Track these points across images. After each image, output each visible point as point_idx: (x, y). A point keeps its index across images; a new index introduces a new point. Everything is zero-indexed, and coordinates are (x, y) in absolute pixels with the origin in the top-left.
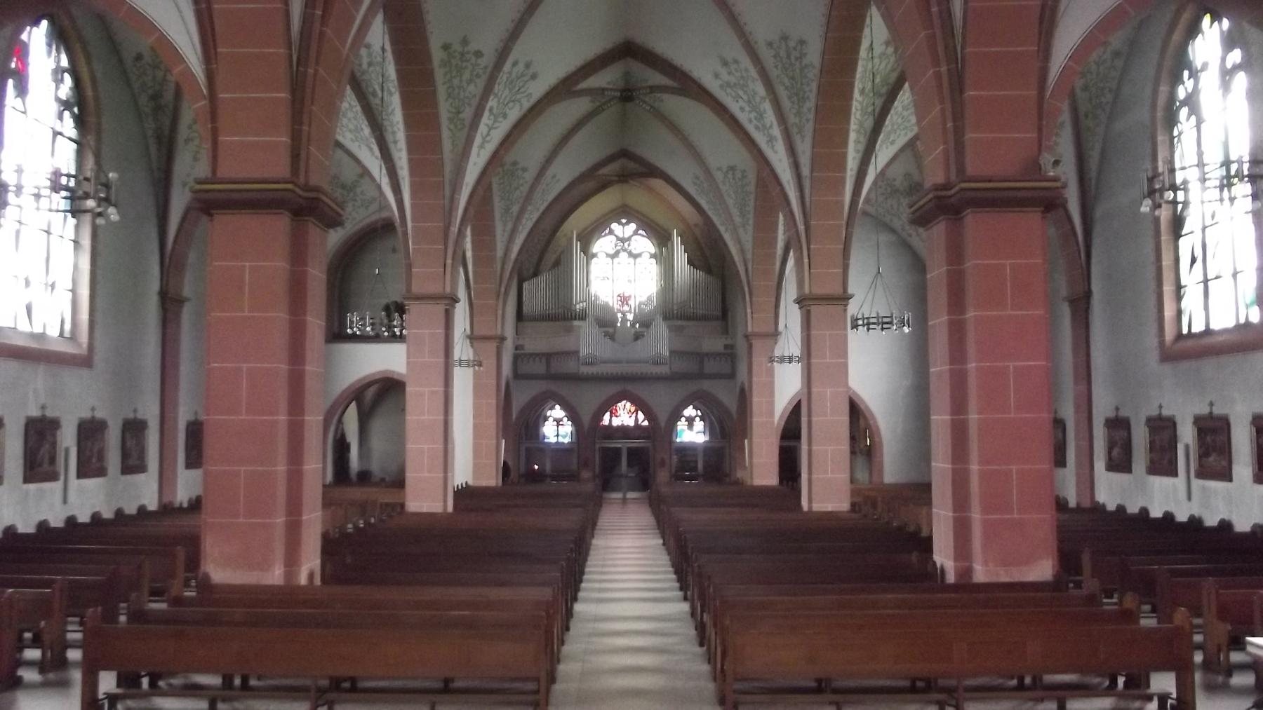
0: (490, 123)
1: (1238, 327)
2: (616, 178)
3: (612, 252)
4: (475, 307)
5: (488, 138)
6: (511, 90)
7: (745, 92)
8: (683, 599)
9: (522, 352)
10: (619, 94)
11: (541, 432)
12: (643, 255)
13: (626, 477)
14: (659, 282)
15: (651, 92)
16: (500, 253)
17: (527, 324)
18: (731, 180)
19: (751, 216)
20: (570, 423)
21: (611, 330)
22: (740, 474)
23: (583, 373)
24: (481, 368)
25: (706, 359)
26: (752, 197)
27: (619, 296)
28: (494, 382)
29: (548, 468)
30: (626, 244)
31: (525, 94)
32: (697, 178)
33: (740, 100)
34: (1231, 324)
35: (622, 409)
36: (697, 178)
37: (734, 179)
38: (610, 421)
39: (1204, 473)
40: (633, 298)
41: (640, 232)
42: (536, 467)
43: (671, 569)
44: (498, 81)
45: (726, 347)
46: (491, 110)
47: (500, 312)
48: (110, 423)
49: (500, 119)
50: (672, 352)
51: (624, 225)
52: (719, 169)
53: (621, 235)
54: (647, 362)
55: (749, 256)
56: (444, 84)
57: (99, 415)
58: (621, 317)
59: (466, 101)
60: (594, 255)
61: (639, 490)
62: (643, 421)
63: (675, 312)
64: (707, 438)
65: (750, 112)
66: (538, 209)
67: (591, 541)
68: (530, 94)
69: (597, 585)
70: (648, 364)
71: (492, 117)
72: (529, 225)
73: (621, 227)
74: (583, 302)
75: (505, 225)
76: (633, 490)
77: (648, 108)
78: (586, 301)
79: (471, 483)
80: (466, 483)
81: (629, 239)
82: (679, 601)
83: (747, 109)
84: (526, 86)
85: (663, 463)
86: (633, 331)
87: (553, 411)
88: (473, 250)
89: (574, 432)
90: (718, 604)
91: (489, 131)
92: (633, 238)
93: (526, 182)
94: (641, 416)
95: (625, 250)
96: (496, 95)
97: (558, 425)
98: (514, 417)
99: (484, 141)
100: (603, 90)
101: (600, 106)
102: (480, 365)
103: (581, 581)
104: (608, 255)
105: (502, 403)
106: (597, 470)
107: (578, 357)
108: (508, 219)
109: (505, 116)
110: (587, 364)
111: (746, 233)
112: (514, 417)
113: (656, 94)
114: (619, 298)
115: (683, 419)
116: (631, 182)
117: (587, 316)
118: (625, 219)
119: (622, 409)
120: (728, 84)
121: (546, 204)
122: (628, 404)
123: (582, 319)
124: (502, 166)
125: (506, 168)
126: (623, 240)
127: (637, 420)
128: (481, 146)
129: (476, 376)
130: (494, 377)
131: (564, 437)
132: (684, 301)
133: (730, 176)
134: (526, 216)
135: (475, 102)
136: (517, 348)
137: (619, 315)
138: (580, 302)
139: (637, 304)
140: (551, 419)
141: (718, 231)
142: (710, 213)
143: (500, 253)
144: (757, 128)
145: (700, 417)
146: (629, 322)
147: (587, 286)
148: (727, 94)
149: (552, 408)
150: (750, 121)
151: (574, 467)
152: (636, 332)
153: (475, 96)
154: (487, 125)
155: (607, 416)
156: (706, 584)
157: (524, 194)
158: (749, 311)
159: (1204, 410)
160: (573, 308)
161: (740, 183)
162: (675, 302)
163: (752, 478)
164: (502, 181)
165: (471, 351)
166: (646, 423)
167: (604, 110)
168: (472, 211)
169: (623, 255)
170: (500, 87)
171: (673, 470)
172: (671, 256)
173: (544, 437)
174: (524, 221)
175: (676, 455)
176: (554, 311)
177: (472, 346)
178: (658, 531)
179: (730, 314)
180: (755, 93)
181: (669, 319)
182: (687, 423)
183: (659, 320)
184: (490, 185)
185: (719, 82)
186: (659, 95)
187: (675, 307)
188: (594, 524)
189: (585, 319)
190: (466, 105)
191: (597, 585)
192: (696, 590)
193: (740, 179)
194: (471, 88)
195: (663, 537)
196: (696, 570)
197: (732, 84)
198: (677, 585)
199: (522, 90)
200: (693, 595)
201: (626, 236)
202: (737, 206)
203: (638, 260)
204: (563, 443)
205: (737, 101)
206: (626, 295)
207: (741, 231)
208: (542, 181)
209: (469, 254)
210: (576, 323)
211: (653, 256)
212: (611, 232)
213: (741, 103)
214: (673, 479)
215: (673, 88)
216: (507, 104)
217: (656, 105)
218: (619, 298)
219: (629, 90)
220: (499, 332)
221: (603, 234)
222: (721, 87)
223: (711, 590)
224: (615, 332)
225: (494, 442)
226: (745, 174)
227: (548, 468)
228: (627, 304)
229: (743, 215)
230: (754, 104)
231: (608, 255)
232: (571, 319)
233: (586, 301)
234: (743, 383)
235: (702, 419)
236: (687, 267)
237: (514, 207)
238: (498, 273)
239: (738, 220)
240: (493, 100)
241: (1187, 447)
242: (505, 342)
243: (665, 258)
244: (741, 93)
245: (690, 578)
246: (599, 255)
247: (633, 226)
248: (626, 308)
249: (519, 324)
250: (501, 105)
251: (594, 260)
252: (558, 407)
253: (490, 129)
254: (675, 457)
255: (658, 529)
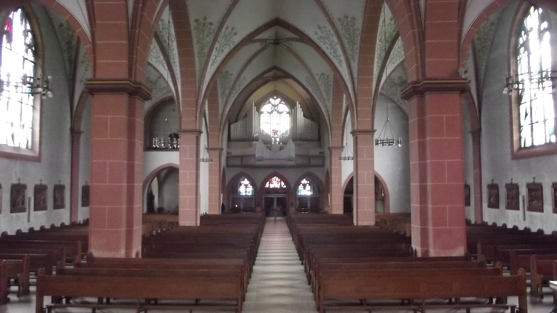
0: (216, 54)
1: (546, 144)
2: (272, 79)
3: (270, 111)
4: (209, 135)
5: (215, 61)
6: (225, 40)
7: (329, 41)
8: (301, 264)
9: (230, 155)
10: (273, 42)
11: (238, 191)
12: (284, 112)
13: (276, 210)
14: (291, 124)
15: (287, 41)
16: (220, 111)
17: (232, 143)
18: (322, 79)
19: (331, 95)
20: (251, 186)
21: (269, 146)
22: (326, 209)
23: (257, 164)
24: (212, 162)
25: (311, 158)
26: (332, 87)
27: (273, 130)
28: (218, 168)
29: (242, 206)
30: (276, 108)
31: (232, 42)
32: (307, 78)
33: (326, 44)
34: (543, 143)
35: (274, 180)
36: (307, 78)
37: (324, 79)
38: (269, 185)
39: (531, 209)
40: (279, 132)
41: (282, 102)
42: (236, 206)
43: (296, 251)
44: (220, 36)
45: (320, 153)
46: (216, 48)
47: (220, 138)
48: (49, 186)
49: (221, 53)
50: (296, 155)
51: (275, 99)
52: (317, 74)
53: (274, 104)
54: (285, 160)
55: (330, 113)
56: (196, 37)
57: (44, 183)
58: (274, 140)
59: (206, 44)
60: (262, 113)
61: (282, 216)
62: (284, 186)
63: (298, 137)
64: (312, 193)
65: (331, 49)
66: (237, 92)
67: (261, 239)
68: (234, 41)
69: (263, 258)
70: (286, 161)
71: (217, 52)
72: (233, 99)
73: (274, 100)
74: (257, 133)
75: (223, 99)
76: (279, 216)
77: (286, 48)
78: (258, 133)
79: (208, 213)
80: (206, 213)
81: (277, 105)
82: (299, 265)
83: (330, 48)
84: (232, 38)
85: (292, 204)
86: (279, 146)
87: (244, 181)
88: (209, 110)
89: (253, 191)
90: (317, 266)
91: (216, 58)
92: (279, 105)
93: (232, 80)
94: (283, 183)
95: (275, 110)
96: (219, 42)
97: (246, 187)
98: (227, 184)
99: (214, 62)
100: (266, 40)
101: (265, 47)
102: (212, 161)
103: (256, 256)
104: (268, 113)
105: (221, 177)
106: (263, 207)
107: (255, 157)
108: (224, 96)
109: (223, 51)
110: (259, 160)
111: (329, 103)
112: (227, 184)
113: (289, 42)
114: (273, 132)
115: (301, 185)
116: (278, 80)
117: (259, 139)
118: (276, 96)
119: (274, 180)
120: (321, 37)
121: (241, 90)
122: (277, 178)
123: (257, 141)
124: (221, 73)
125: (223, 74)
126: (275, 106)
127: (281, 185)
128: (212, 65)
129: (210, 166)
130: (218, 166)
131: (249, 193)
132: (302, 133)
133: (322, 77)
134: (232, 95)
135: (209, 45)
136: (228, 153)
137: (273, 139)
138: (256, 133)
139: (281, 134)
140: (243, 185)
141: (317, 102)
142: (313, 94)
143: (220, 111)
144: (334, 56)
145: (309, 184)
146: (277, 142)
147: (259, 126)
148: (321, 42)
149: (243, 180)
150: (331, 53)
151: (253, 206)
152: (280, 146)
153: (209, 42)
154: (215, 55)
155: (268, 184)
156: (311, 258)
157: (231, 86)
158: (330, 137)
159: (531, 181)
160: (253, 136)
161: (326, 81)
162: (298, 133)
163: (331, 211)
164: (221, 80)
165: (208, 155)
166: (285, 186)
167: (266, 48)
168: (208, 93)
169: (275, 112)
170: (221, 38)
171: (297, 207)
172: (296, 113)
173: (240, 193)
174: (231, 97)
175: (298, 200)
176: (244, 137)
177: (208, 153)
178: (290, 234)
179: (322, 138)
180: (333, 41)
181: (295, 141)
182: (303, 187)
183: (291, 141)
184: (216, 82)
185: (317, 36)
186: (291, 42)
187: (298, 136)
188: (262, 231)
189: (258, 141)
190: (206, 46)
191: (263, 258)
192: (307, 260)
193: (326, 79)
194: (208, 39)
195: (292, 237)
196: (307, 251)
197: (323, 37)
198: (299, 258)
199: (230, 40)
200: (306, 262)
201: (276, 104)
202: (325, 91)
203: (282, 115)
204: (248, 195)
205: (325, 45)
206: (276, 130)
207: (327, 102)
208: (239, 80)
209: (207, 112)
210: (254, 142)
211: (288, 113)
212: (270, 102)
213: (327, 45)
214: (297, 211)
215: (297, 39)
216: (224, 46)
217: (289, 46)
218: (273, 132)
219: (277, 40)
220: (220, 146)
221: (266, 103)
222: (318, 38)
223: (314, 260)
224: (271, 146)
225: (218, 195)
226: (329, 77)
227: (242, 206)
228: (277, 134)
229: (328, 95)
230: (333, 46)
231: (268, 113)
232: (252, 141)
233: (258, 133)
234: (327, 169)
235: (310, 185)
236: (303, 118)
237: (227, 91)
238: (220, 120)
239: (325, 97)
240: (217, 44)
241: (523, 197)
242: (223, 151)
243: (293, 114)
244: (327, 41)
245: (304, 255)
246: (264, 112)
247: (279, 100)
248: (276, 136)
249: (229, 143)
250: (221, 46)
251: (262, 115)
252: (246, 179)
253: (216, 57)
254: (298, 201)
255: (290, 233)
